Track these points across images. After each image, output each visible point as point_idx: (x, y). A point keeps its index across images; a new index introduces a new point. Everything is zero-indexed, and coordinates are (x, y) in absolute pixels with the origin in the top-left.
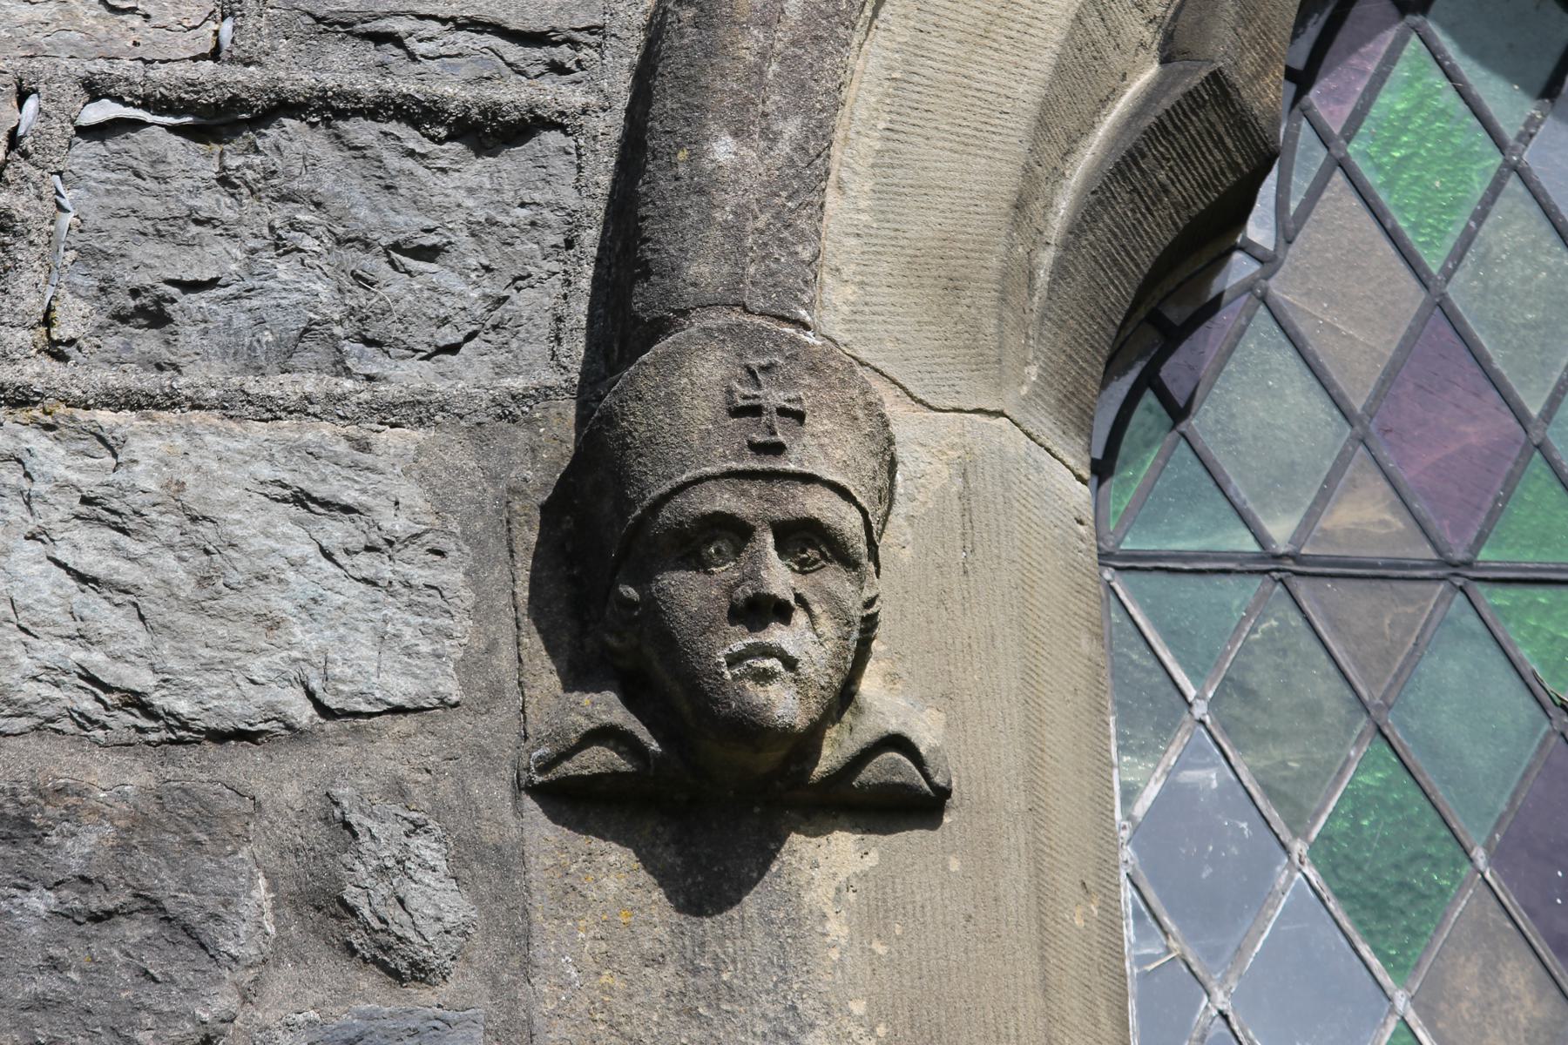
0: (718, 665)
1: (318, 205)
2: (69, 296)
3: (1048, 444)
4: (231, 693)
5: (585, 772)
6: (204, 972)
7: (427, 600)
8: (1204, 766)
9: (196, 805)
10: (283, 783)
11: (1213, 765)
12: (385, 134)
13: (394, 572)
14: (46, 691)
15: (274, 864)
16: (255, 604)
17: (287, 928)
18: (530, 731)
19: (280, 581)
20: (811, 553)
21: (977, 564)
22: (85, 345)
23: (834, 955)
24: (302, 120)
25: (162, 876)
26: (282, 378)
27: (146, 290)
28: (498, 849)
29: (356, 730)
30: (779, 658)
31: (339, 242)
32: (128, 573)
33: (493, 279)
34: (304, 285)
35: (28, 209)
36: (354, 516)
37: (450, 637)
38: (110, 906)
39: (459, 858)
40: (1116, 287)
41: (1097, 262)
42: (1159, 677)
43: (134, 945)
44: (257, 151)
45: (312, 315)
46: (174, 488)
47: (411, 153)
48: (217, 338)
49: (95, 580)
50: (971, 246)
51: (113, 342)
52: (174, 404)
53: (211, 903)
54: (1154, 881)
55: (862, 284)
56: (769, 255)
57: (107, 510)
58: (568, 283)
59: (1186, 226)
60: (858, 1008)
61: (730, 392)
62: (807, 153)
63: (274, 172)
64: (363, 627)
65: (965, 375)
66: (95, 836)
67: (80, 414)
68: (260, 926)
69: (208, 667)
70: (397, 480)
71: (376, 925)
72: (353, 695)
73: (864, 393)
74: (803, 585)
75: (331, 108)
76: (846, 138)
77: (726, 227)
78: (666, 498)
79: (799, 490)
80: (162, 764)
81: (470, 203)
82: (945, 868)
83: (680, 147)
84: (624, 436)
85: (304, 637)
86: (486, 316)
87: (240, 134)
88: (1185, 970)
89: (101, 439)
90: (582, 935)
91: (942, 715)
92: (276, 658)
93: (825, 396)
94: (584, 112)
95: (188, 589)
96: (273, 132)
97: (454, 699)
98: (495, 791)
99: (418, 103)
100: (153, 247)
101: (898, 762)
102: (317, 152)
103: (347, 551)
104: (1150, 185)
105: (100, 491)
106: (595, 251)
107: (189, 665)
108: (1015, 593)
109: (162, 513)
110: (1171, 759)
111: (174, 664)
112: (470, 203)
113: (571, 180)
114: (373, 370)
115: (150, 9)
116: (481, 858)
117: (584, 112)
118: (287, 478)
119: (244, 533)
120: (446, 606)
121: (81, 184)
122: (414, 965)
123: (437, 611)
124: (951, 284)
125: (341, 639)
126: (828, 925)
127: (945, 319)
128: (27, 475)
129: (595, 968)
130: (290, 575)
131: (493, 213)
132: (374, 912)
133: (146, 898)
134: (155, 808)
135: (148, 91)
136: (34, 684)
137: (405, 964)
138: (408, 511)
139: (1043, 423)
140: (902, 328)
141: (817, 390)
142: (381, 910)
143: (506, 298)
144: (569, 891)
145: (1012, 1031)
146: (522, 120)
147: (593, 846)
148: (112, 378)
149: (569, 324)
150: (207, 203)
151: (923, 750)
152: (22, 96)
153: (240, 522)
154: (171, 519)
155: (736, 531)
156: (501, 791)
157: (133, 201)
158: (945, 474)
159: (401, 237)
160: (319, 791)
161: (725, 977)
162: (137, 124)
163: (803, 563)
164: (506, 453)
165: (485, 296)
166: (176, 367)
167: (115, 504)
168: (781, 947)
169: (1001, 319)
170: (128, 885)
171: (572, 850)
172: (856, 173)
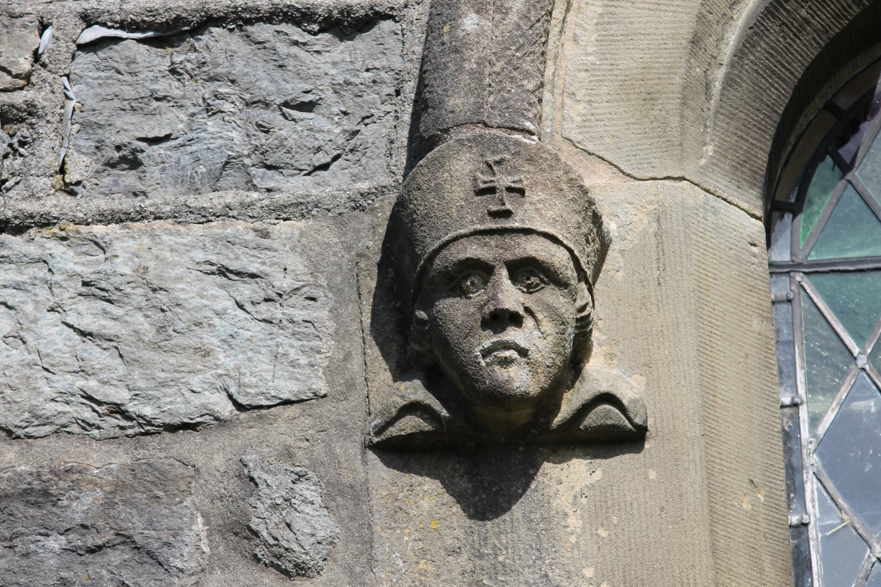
0: (476, 357)
1: (233, 81)
2: (76, 154)
3: (725, 196)
4: (178, 400)
5: (403, 433)
6: (161, 580)
7: (304, 330)
8: (867, 398)
9: (156, 473)
10: (212, 455)
11: (873, 397)
12: (278, 32)
13: (283, 314)
14: (61, 407)
15: (207, 507)
16: (193, 342)
17: (217, 548)
18: (372, 409)
19: (210, 325)
20: (534, 280)
21: (667, 278)
22: (88, 184)
23: (573, 539)
24: (224, 28)
25: (134, 520)
26: (212, 195)
27: (125, 146)
28: (352, 487)
29: (260, 417)
30: (515, 349)
31: (247, 104)
32: (111, 328)
33: (349, 119)
34: (225, 134)
35: (45, 100)
36: (257, 280)
37: (319, 352)
38: (100, 543)
39: (328, 494)
40: (776, 89)
41: (758, 73)
42: (835, 343)
43: (116, 566)
44: (196, 50)
45: (230, 153)
46: (141, 271)
47: (296, 43)
48: (171, 172)
49: (91, 334)
50: (663, 70)
51: (107, 181)
52: (143, 217)
53: (165, 536)
54: (832, 475)
55: (590, 102)
56: (503, 89)
57: (99, 288)
58: (397, 118)
59: (827, 45)
60: (589, 572)
61: (475, 179)
62: (529, 20)
63: (204, 63)
64: (263, 350)
65: (658, 155)
66: (91, 498)
67: (83, 229)
68: (198, 548)
69: (163, 384)
70: (286, 254)
71: (272, 542)
73: (567, 173)
74: (530, 301)
75: (241, 18)
76: (579, 8)
77: (472, 73)
78: (437, 252)
79: (522, 240)
80: (136, 449)
81: (333, 72)
82: (646, 478)
83: (445, 23)
84: (412, 214)
85: (225, 359)
86: (346, 144)
87: (184, 40)
88: (855, 533)
89: (97, 244)
90: (406, 538)
91: (644, 378)
92: (208, 375)
93: (539, 177)
94: (406, 6)
95: (150, 335)
96: (205, 37)
97: (323, 392)
99: (298, 10)
100: (130, 118)
102: (233, 47)
103: (253, 303)
104: (795, 19)
105: (93, 277)
106: (413, 96)
107: (152, 384)
108: (692, 295)
109: (134, 288)
110: (843, 394)
111: (141, 384)
112: (333, 72)
113: (398, 52)
114: (271, 184)
116: (342, 494)
117: (406, 6)
118: (214, 258)
119: (186, 296)
120: (317, 333)
121: (82, 81)
122: (297, 566)
123: (311, 336)
124: (649, 97)
125: (250, 359)
126: (569, 520)
127: (645, 120)
128: (50, 270)
129: (415, 559)
130: (216, 321)
131: (348, 77)
132: (270, 534)
133: (123, 535)
134: (130, 477)
135: (123, 18)
137: (291, 566)
139: (720, 183)
140: (616, 128)
141: (534, 173)
142: (275, 532)
143: (358, 131)
144: (397, 512)
145: (692, 581)
146: (367, 15)
147: (413, 481)
148: (104, 204)
149: (396, 145)
150: (163, 86)
152: (43, 27)
153: (183, 290)
154: (139, 291)
155: (482, 270)
156: (354, 449)
157: (115, 90)
158: (646, 221)
159: (289, 98)
160: (236, 458)
161: (501, 559)
162: (117, 40)
163: (529, 287)
164: (357, 231)
165: (345, 131)
166: (144, 193)
167: (103, 285)
168: (538, 537)
169: (682, 116)
170: (111, 528)
171: (400, 484)
172: (585, 30)
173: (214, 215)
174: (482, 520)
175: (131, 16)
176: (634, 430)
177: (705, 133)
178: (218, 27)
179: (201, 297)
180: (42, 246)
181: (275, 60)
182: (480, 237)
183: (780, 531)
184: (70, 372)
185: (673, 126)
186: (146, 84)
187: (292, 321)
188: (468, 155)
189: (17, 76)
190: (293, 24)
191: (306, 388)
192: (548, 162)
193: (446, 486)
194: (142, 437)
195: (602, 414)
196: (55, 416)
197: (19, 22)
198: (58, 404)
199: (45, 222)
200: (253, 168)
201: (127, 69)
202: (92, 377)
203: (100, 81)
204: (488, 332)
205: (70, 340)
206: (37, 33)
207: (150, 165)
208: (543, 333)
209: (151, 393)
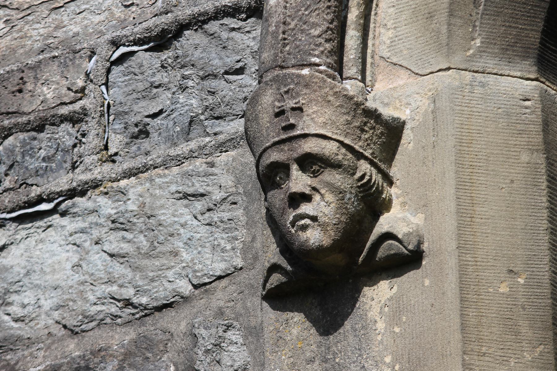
0: (288, 228)
2: (113, 135)
5: (273, 286)
7: (229, 226)
10: (177, 322)
12: (222, 25)
14: (99, 308)
19: (178, 234)
23: (379, 338)
24: (192, 29)
27: (139, 123)
29: (206, 291)
37: (237, 240)
45: (192, 114)
47: (233, 29)
57: (119, 223)
63: (177, 57)
67: (115, 185)
69: (152, 280)
72: (203, 276)
73: (332, 89)
75: (199, 21)
82: (423, 285)
90: (284, 357)
91: (423, 215)
92: (177, 269)
93: (313, 96)
97: (240, 266)
98: (255, 302)
100: (143, 103)
101: (391, 244)
107: (146, 282)
109: (138, 219)
111: (140, 283)
112: (252, 44)
114: (217, 129)
115: (138, 2)
118: (180, 189)
121: (116, 85)
123: (233, 229)
124: (429, 16)
127: (427, 32)
130: (182, 231)
134: (134, 347)
136: (95, 307)
138: (225, 188)
139: (490, 63)
141: (309, 94)
145: (448, 352)
150: (161, 77)
151: (400, 236)
153: (163, 214)
154: (142, 220)
156: (257, 300)
157: (134, 87)
158: (427, 104)
161: (337, 360)
162: (132, 53)
163: (313, 172)
167: (121, 220)
169: (449, 24)
171: (281, 320)
173: (185, 158)
174: (327, 335)
175: (138, 36)
176: (409, 254)
177: (474, 30)
178: (188, 30)
179: (174, 216)
180: (95, 201)
181: (221, 44)
182: (278, 146)
183: (540, 301)
184: (103, 283)
185: (443, 33)
186: (149, 79)
187: (222, 222)
188: (270, 91)
189: (76, 92)
190: (231, 17)
191: (230, 265)
192: (318, 84)
193: (307, 316)
194: (144, 318)
195: (387, 248)
196: (96, 314)
197: (77, 55)
198: (98, 306)
199: (95, 185)
200: (206, 121)
201: (139, 71)
202: (114, 284)
203: (126, 83)
204: (292, 209)
205: (105, 261)
206: (87, 60)
207: (153, 133)
208: (327, 203)
209: (145, 288)
